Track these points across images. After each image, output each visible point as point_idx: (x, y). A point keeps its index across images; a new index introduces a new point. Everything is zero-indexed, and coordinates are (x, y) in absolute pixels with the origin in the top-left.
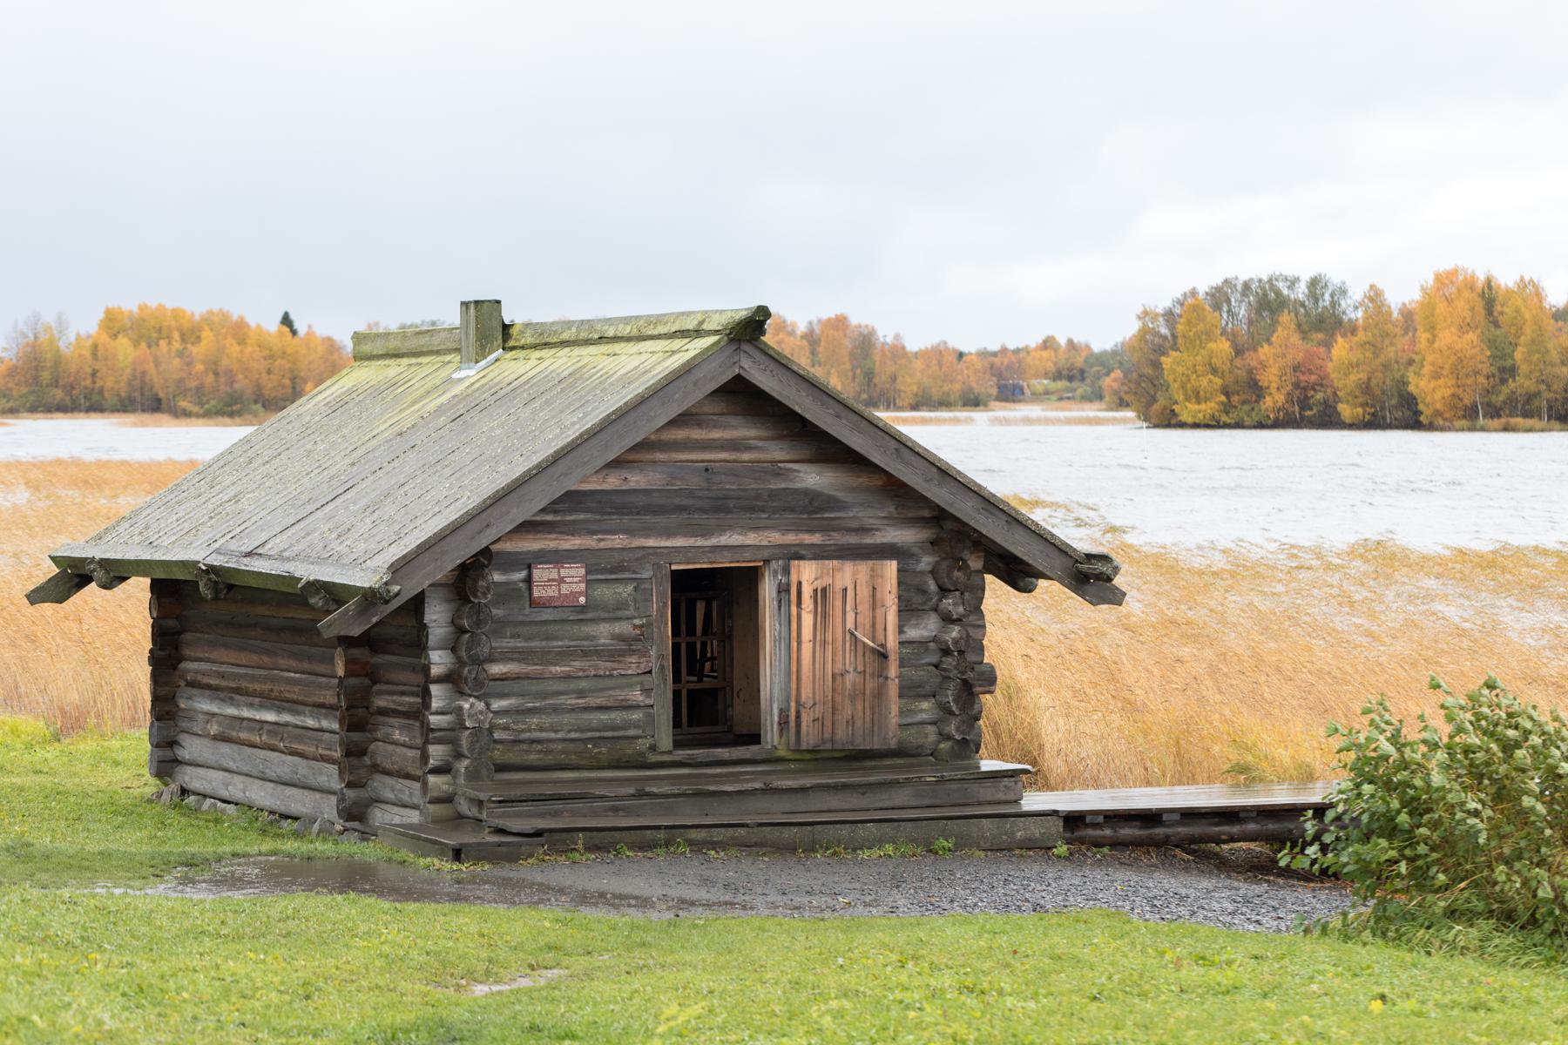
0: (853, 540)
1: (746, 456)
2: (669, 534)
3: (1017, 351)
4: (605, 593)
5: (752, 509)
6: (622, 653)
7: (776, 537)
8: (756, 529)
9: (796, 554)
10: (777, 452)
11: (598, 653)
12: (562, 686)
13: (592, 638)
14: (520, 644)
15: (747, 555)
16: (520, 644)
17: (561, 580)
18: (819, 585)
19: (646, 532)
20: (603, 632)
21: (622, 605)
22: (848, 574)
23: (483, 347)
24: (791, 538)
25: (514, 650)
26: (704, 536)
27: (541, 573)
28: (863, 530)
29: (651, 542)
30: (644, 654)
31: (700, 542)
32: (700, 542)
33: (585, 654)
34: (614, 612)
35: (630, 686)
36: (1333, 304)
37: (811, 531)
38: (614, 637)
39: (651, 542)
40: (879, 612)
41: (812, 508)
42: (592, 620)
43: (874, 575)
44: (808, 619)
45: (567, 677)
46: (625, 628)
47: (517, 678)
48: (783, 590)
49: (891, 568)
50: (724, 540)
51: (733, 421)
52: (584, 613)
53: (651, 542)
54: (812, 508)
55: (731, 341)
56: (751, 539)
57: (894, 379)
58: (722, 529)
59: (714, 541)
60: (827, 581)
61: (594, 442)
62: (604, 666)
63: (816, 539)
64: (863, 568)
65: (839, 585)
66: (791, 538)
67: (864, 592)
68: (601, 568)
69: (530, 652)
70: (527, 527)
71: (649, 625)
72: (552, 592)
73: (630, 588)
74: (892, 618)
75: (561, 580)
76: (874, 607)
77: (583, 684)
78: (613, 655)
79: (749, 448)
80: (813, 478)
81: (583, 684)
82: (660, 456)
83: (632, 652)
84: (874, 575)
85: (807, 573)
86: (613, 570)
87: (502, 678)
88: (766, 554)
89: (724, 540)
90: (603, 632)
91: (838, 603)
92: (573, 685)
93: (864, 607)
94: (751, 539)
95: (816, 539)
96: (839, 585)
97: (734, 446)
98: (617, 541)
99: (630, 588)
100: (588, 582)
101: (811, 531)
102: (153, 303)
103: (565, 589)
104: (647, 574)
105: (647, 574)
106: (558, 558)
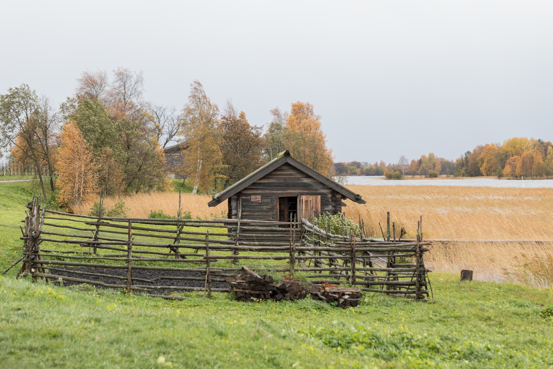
0: (315, 192)
1: (292, 177)
2: (278, 190)
3: (513, 139)
4: (265, 201)
5: (294, 186)
6: (269, 211)
7: (299, 191)
8: (295, 190)
9: (303, 194)
10: (299, 176)
11: (264, 211)
12: (257, 217)
13: (263, 208)
14: (249, 209)
15: (293, 194)
16: (249, 209)
17: (256, 198)
18: (306, 200)
19: (273, 190)
20: (265, 207)
21: (268, 203)
22: (311, 198)
23: (273, 157)
24: (302, 191)
25: (248, 210)
26: (284, 191)
27: (253, 197)
28: (316, 190)
29: (274, 192)
30: (273, 211)
31: (284, 192)
32: (284, 192)
33: (262, 211)
34: (267, 204)
35: (270, 217)
36: (498, 148)
37: (306, 190)
38: (267, 208)
39: (274, 192)
40: (317, 205)
41: (305, 186)
42: (263, 205)
43: (316, 198)
44: (304, 206)
45: (258, 215)
46: (269, 207)
47: (249, 215)
48: (300, 200)
49: (319, 197)
50: (289, 191)
51: (290, 170)
52: (261, 204)
53: (274, 192)
54: (305, 186)
55: (285, 156)
56: (294, 191)
57: (130, 196)
58: (288, 190)
59: (286, 192)
60: (307, 199)
61: (259, 174)
62: (265, 213)
63: (307, 191)
64: (314, 197)
65: (310, 200)
66: (302, 191)
67: (314, 201)
68: (264, 196)
69: (251, 211)
70: (246, 189)
71: (274, 206)
72: (254, 200)
73: (270, 200)
74: (319, 206)
75: (256, 198)
76: (316, 204)
77: (261, 216)
78: (267, 212)
79: (293, 175)
80: (306, 181)
81: (261, 216)
82: (276, 177)
83: (271, 211)
84: (316, 198)
85: (304, 198)
86: (267, 197)
87: (246, 215)
88: (297, 194)
89: (289, 191)
90: (265, 207)
91: (309, 203)
92: (259, 217)
93: (314, 204)
94: (294, 191)
95: (307, 191)
96: (310, 200)
97: (290, 175)
98: (267, 191)
99: (270, 200)
100: (262, 199)
101: (306, 190)
102: (342, 162)
103: (257, 200)
104: (274, 197)
105: (274, 197)
106: (256, 194)
